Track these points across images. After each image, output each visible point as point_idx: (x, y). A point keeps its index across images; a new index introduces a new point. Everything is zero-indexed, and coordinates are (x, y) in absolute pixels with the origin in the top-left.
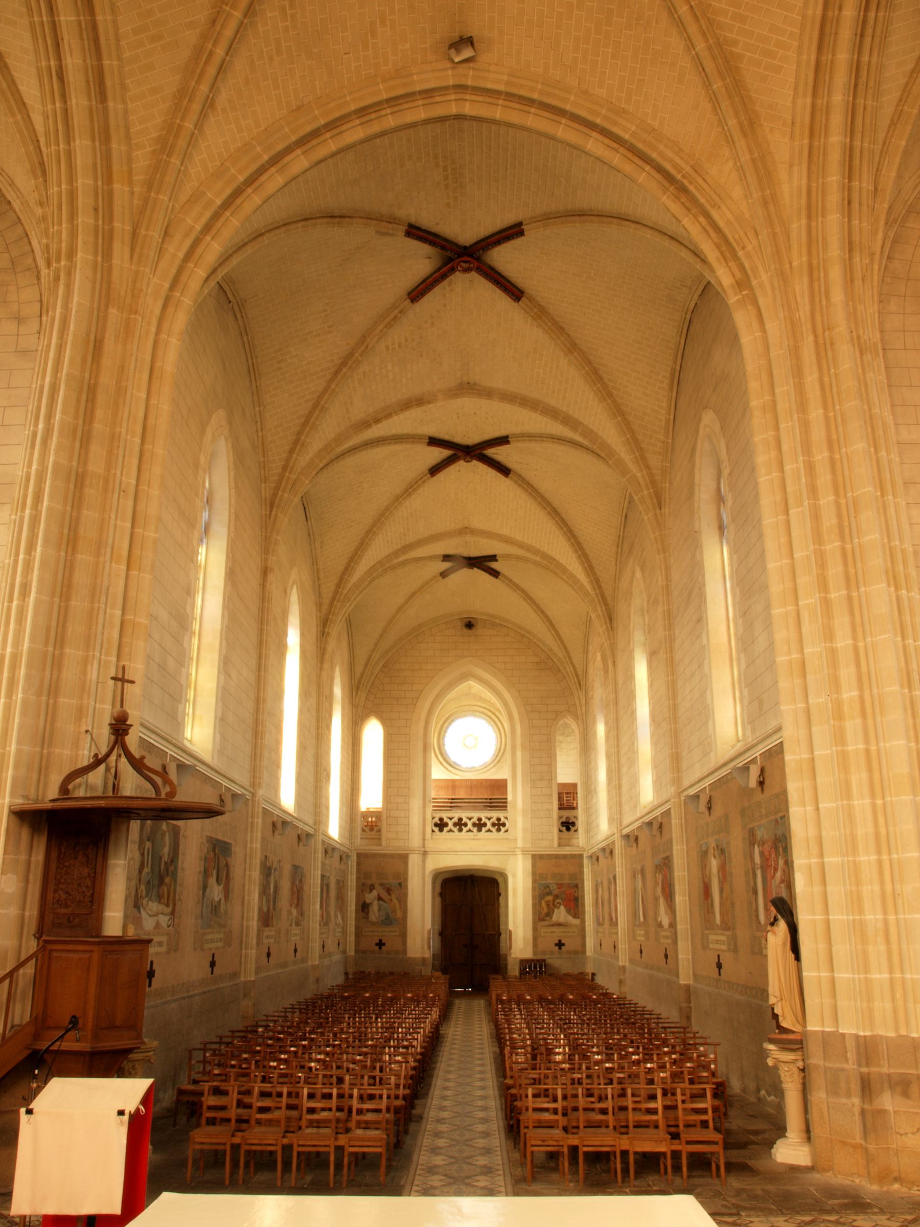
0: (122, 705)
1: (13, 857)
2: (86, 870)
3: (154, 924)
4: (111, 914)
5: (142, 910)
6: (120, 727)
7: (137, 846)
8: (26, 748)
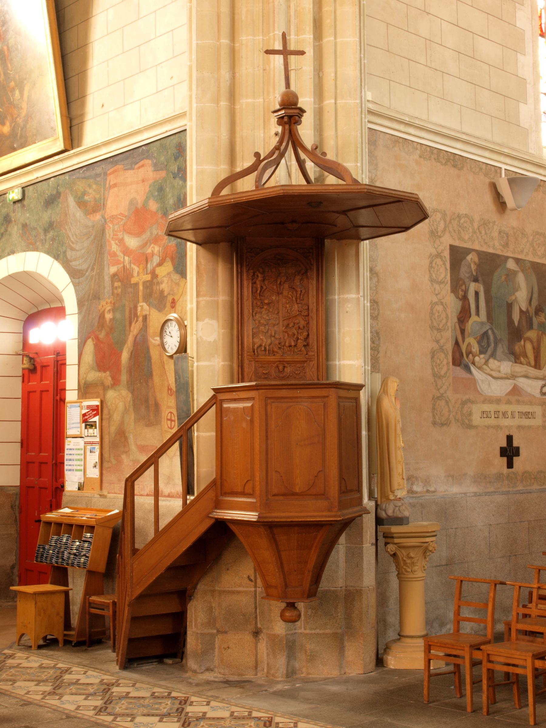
0: (288, 85)
1: (208, 298)
2: (296, 307)
3: (510, 388)
4: (346, 362)
5: (473, 369)
6: (290, 114)
7: (448, 287)
8: (209, 168)
